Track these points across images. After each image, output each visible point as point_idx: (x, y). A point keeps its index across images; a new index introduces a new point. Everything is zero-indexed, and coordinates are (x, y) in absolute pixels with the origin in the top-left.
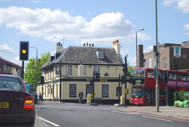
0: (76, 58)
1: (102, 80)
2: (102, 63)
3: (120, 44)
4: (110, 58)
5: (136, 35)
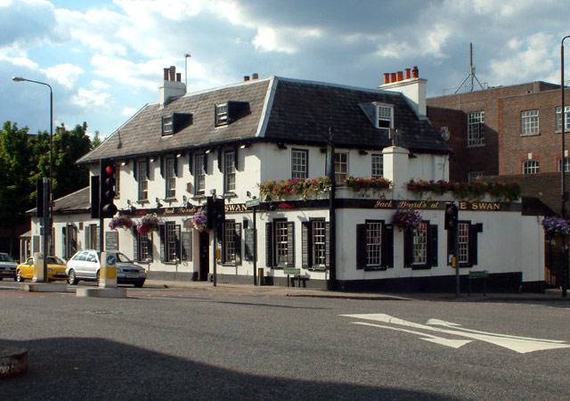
0: (314, 121)
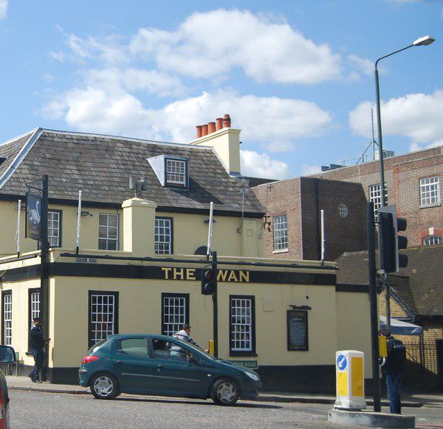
0: (77, 177)
1: (229, 272)
2: (184, 202)
3: (237, 132)
4: (209, 187)
5: (377, 72)
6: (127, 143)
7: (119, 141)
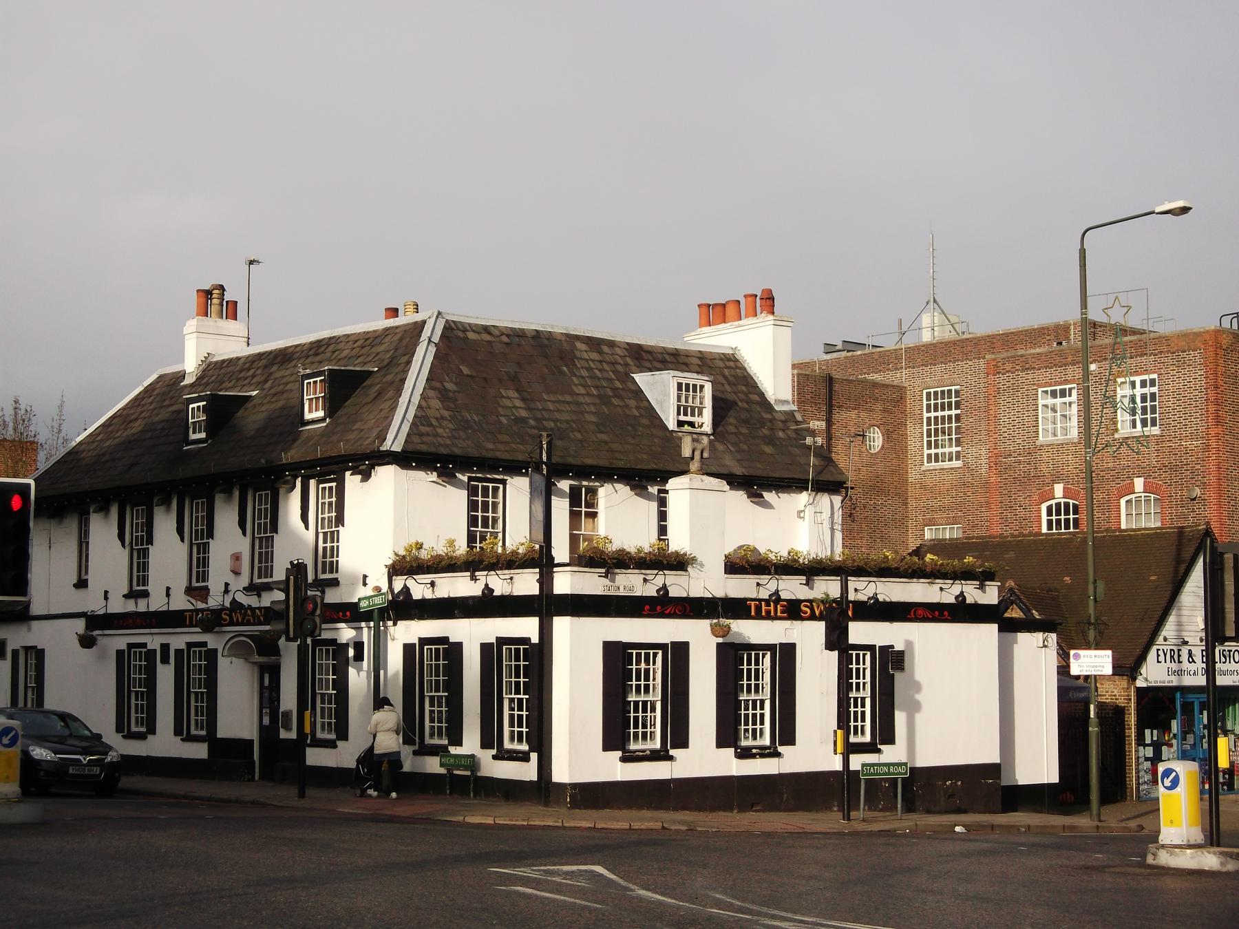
0: (524, 414)
5: (1083, 252)
6: (595, 343)
7: (578, 337)
